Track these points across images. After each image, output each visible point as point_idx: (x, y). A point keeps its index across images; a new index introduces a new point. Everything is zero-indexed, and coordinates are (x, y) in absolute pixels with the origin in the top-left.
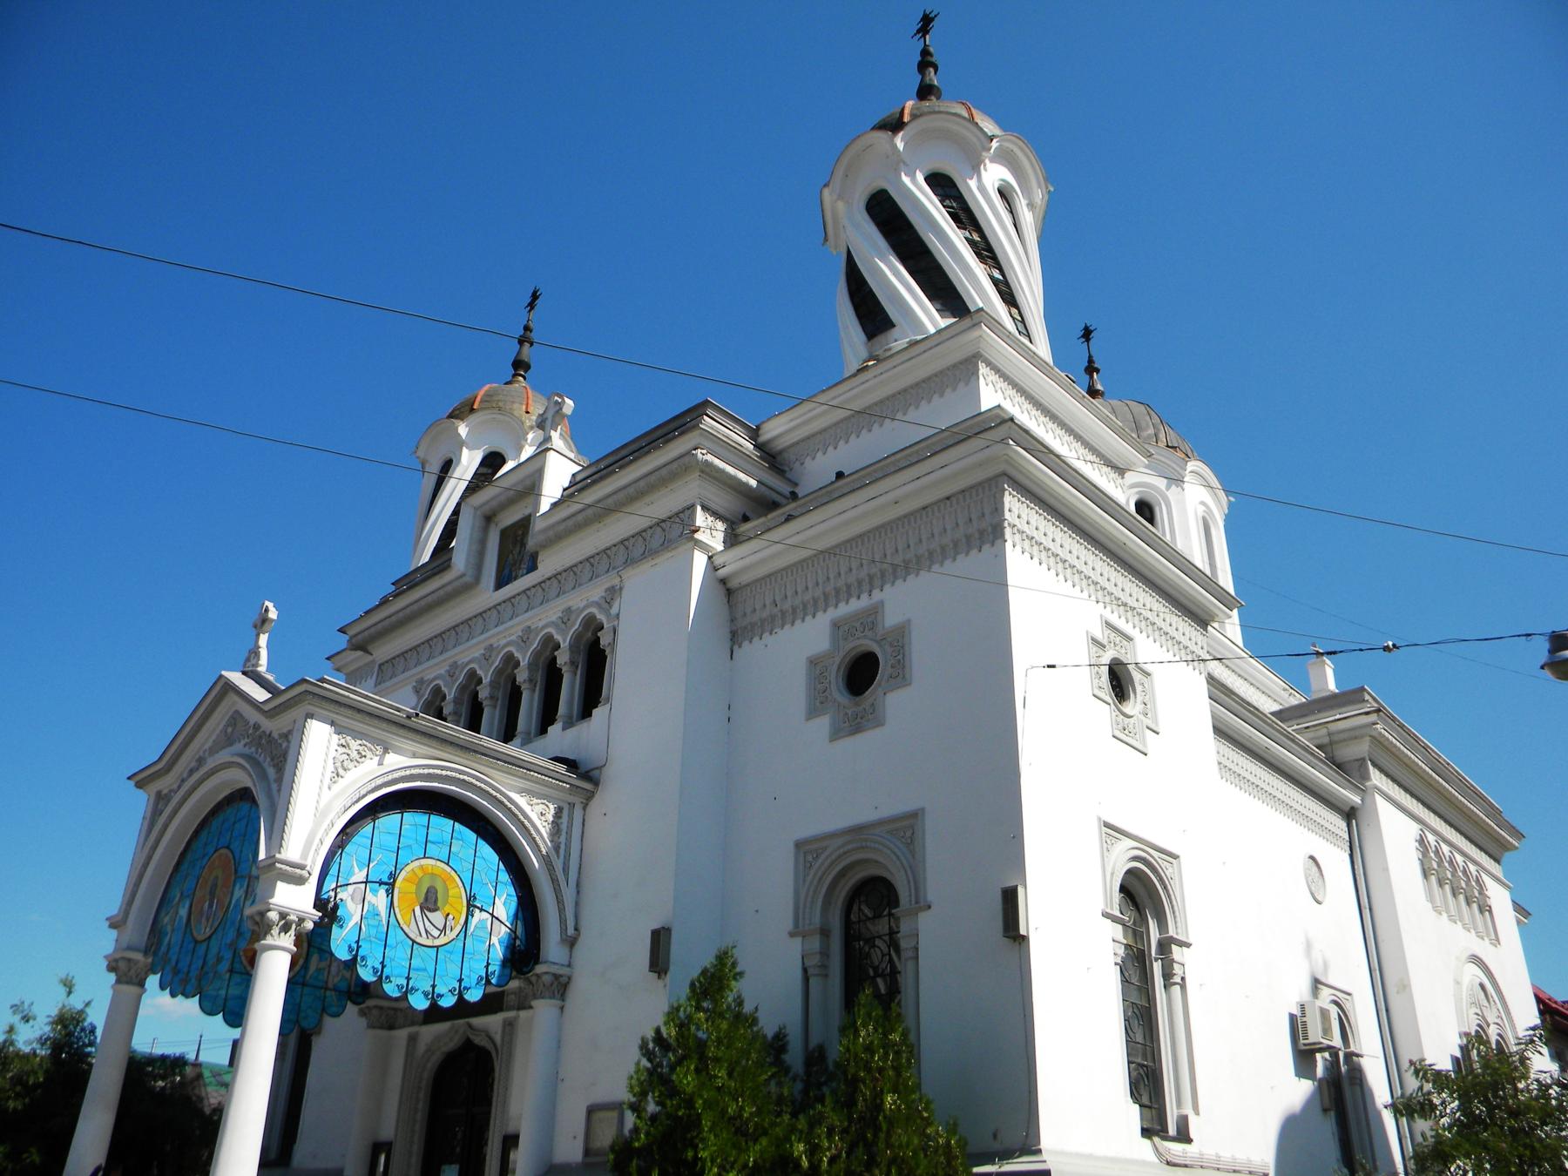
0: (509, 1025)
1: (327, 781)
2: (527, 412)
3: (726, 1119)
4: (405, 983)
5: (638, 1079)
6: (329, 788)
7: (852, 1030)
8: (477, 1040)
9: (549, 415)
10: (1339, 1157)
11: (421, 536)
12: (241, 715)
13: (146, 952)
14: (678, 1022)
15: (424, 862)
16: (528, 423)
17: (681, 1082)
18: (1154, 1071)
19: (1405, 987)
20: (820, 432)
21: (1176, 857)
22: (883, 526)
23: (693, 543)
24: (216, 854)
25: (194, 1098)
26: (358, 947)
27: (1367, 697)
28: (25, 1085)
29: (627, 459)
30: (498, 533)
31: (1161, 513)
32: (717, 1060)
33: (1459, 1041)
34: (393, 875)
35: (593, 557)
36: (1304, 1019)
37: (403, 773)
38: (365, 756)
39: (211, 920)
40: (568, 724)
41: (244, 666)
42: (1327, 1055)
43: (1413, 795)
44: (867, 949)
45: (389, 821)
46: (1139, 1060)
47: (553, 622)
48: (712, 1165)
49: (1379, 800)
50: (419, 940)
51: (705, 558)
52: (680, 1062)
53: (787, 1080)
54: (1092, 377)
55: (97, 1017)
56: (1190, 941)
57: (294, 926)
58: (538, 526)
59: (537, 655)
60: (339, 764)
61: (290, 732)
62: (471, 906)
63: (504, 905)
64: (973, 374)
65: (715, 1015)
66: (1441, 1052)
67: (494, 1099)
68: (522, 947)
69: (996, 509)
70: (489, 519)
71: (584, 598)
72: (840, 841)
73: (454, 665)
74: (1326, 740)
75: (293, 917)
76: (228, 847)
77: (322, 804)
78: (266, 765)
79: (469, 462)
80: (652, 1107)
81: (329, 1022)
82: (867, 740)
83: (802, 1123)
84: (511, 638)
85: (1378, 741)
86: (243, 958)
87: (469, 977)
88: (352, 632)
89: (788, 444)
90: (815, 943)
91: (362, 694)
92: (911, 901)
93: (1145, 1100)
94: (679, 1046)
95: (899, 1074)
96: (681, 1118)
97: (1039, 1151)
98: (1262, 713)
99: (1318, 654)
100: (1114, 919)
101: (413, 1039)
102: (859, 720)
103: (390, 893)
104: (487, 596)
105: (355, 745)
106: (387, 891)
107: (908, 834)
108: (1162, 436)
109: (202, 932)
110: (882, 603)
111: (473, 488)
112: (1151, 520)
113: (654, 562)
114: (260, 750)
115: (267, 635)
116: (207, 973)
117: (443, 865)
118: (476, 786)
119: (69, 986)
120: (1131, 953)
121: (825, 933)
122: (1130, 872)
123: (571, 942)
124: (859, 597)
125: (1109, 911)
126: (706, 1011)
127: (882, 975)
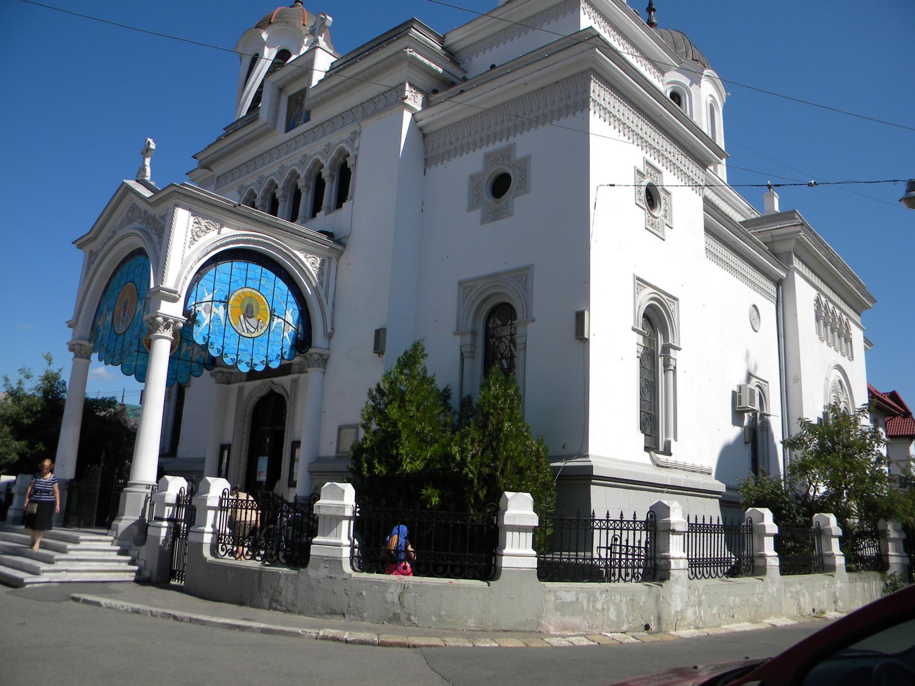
0: (295, 382)
1: (188, 244)
2: (304, 25)
3: (415, 433)
4: (235, 357)
5: (367, 411)
6: (190, 247)
7: (487, 387)
8: (277, 390)
9: (317, 27)
10: (751, 468)
11: (240, 100)
12: (137, 206)
13: (90, 341)
14: (389, 380)
15: (245, 290)
16: (304, 32)
17: (390, 413)
18: (654, 417)
19: (798, 380)
20: (482, 40)
21: (676, 299)
22: (518, 97)
23: (403, 106)
24: (126, 285)
25: (122, 421)
26: (209, 337)
27: (796, 216)
28: (31, 412)
29: (364, 54)
30: (287, 98)
31: (686, 100)
32: (410, 401)
33: (823, 410)
34: (228, 298)
35: (343, 113)
36: (740, 394)
37: (232, 239)
38: (210, 229)
39: (125, 323)
40: (329, 212)
41: (137, 177)
42: (751, 414)
43: (816, 274)
44: (497, 343)
45: (225, 267)
46: (646, 411)
47: (319, 152)
48: (407, 457)
49: (796, 275)
50: (243, 334)
51: (410, 115)
52: (390, 402)
53: (450, 414)
54: (650, 14)
55: (66, 377)
56: (680, 347)
57: (172, 326)
58: (310, 94)
59: (310, 171)
60: (194, 234)
61: (166, 215)
62: (272, 315)
63: (291, 315)
64: (576, 7)
65: (411, 377)
66: (813, 411)
67: (287, 421)
68: (302, 339)
69: (585, 90)
70: (281, 90)
71: (338, 138)
73: (262, 177)
74: (770, 240)
75: (171, 320)
76: (132, 282)
77: (186, 257)
78: (152, 234)
79: (269, 54)
80: (374, 426)
81: (194, 380)
82: (502, 224)
83: (457, 437)
84: (295, 161)
85: (800, 242)
86: (144, 345)
87: (272, 355)
88: (200, 158)
89: (461, 47)
90: (468, 339)
91: (209, 194)
92: (523, 317)
93: (648, 432)
94: (390, 393)
95: (512, 412)
96: (390, 432)
97: (588, 456)
98: (734, 222)
99: (769, 187)
100: (638, 332)
101: (241, 389)
102: (498, 212)
103: (226, 307)
104: (280, 136)
105: (203, 222)
106: (224, 306)
107: (524, 279)
108: (690, 53)
109: (120, 329)
110: (515, 144)
111: (270, 72)
112: (679, 104)
113: (378, 117)
114: (148, 226)
115: (150, 158)
116: (124, 352)
117: (255, 292)
118: (274, 246)
119: (50, 361)
120: (647, 352)
121: (474, 333)
122: (649, 306)
123: (330, 336)
124: (501, 141)
125: (636, 327)
126: (405, 375)
127: (506, 358)
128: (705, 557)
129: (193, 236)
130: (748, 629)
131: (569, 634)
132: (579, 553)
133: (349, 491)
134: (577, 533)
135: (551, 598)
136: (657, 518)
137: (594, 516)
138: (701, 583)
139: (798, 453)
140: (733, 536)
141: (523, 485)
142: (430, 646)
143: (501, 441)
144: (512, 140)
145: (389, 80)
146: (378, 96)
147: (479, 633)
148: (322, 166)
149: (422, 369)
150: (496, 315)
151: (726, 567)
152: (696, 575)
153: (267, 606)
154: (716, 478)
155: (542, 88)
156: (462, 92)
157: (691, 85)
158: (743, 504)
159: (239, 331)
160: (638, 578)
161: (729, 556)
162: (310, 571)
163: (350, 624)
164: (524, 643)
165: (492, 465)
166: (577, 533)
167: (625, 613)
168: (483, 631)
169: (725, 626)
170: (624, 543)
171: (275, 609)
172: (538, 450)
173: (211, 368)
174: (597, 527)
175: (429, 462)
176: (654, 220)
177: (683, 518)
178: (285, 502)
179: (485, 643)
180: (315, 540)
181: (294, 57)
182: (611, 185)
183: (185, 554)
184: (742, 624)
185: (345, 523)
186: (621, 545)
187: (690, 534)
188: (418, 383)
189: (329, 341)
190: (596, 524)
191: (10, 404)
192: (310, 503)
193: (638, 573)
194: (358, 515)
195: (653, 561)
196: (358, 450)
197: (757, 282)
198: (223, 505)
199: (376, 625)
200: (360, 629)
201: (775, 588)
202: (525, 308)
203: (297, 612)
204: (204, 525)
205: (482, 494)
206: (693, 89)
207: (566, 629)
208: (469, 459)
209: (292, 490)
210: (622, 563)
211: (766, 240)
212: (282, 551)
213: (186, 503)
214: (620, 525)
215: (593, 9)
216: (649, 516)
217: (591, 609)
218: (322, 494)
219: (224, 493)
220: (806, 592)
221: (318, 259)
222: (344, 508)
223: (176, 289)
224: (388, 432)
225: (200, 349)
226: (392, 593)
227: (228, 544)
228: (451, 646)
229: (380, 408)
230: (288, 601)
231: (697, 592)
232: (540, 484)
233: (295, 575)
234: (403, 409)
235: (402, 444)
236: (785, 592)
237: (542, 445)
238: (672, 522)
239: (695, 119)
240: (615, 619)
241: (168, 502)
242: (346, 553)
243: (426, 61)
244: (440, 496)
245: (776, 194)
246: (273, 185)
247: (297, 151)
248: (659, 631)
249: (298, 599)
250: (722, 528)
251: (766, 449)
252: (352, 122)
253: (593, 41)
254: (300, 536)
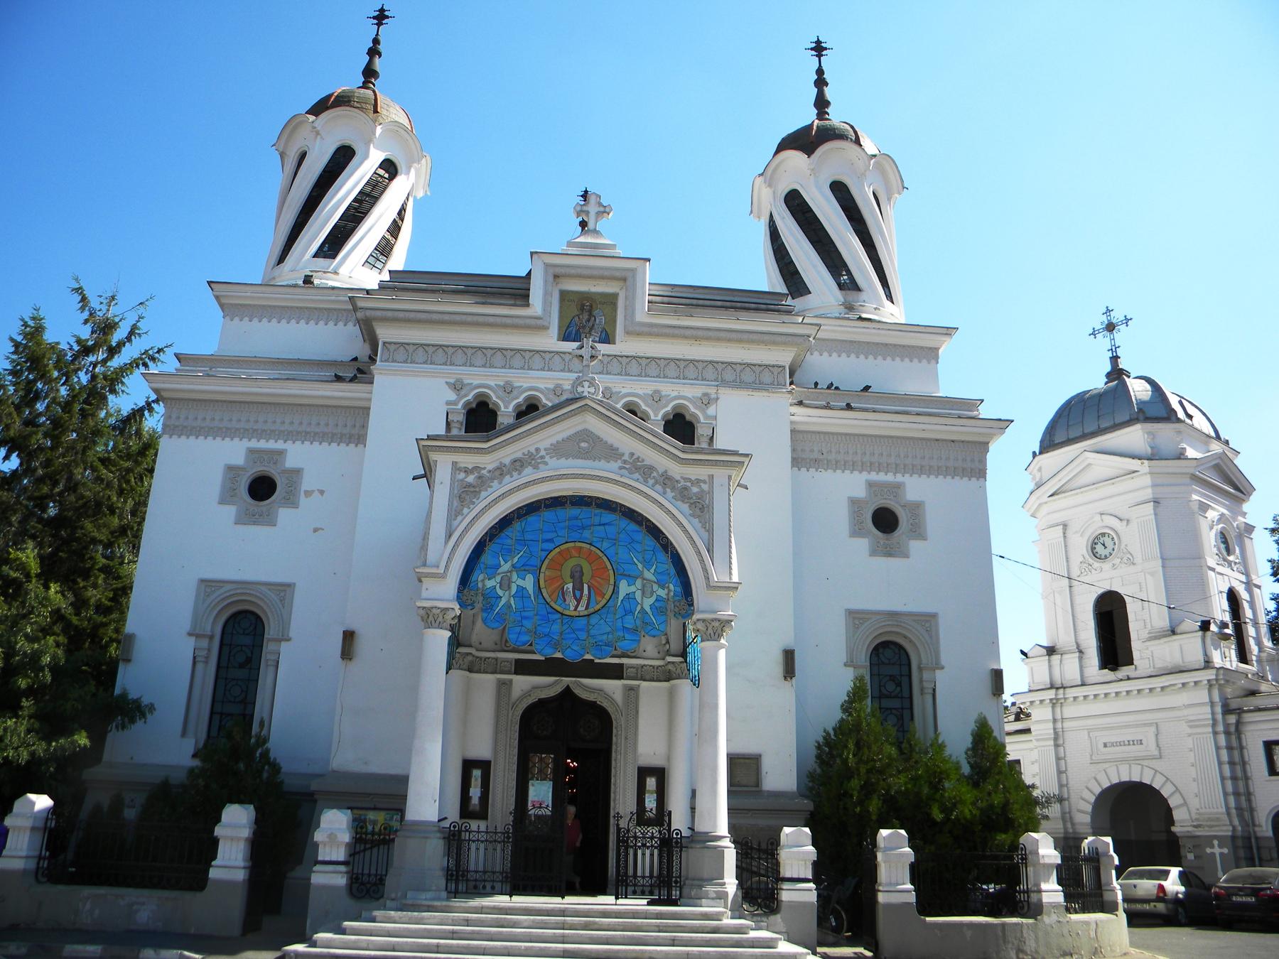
72: (234, 586)
191: (895, 756)
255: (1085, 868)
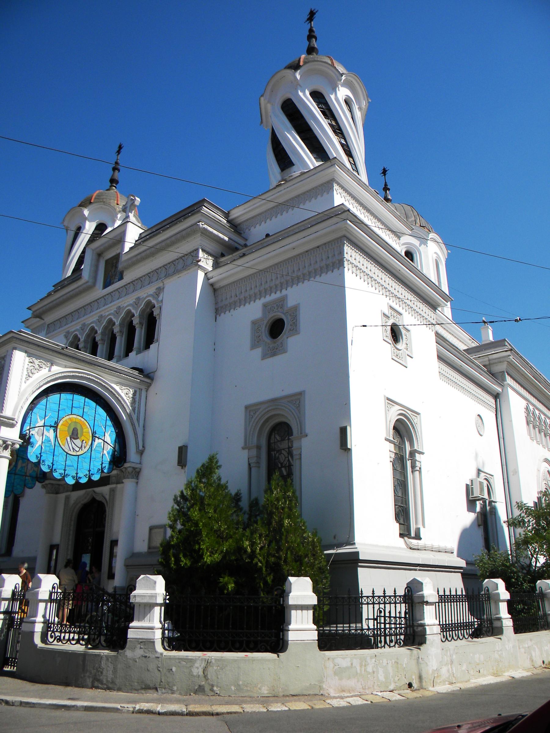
0: (113, 491)
1: (24, 379)
2: (118, 204)
4: (63, 472)
5: (173, 514)
6: (25, 382)
14: (191, 488)
18: (406, 509)
19: (516, 472)
20: (258, 215)
21: (418, 414)
26: (41, 456)
27: (506, 344)
31: (417, 257)
32: (209, 505)
33: (537, 495)
34: (57, 423)
35: (150, 273)
36: (472, 486)
37: (60, 375)
38: (42, 367)
40: (139, 352)
42: (481, 502)
45: (54, 398)
46: (399, 504)
47: (131, 304)
48: (207, 552)
49: (510, 391)
50: (69, 452)
51: (203, 274)
52: (192, 506)
53: (241, 513)
54: (386, 192)
57: (10, 447)
58: (123, 258)
59: (123, 319)
60: (29, 371)
61: (5, 356)
62: (94, 436)
63: (110, 436)
65: (208, 485)
67: (106, 524)
68: (118, 455)
69: (341, 253)
70: (100, 255)
74: (487, 363)
75: (9, 443)
79: (90, 227)
80: (179, 526)
83: (248, 533)
85: (510, 364)
90: (254, 452)
91: (40, 338)
93: (402, 522)
94: (192, 499)
96: (193, 531)
97: (354, 544)
98: (459, 350)
101: (67, 498)
102: (275, 350)
103: (55, 431)
104: (99, 292)
106: (54, 430)
107: (298, 403)
108: (418, 221)
110: (286, 296)
111: (90, 241)
117: (80, 418)
118: (95, 381)
121: (259, 447)
122: (397, 420)
123: (141, 453)
124: (276, 293)
125: (388, 438)
126: (204, 483)
127: (285, 467)
128: (453, 622)
129: (28, 373)
130: (492, 682)
131: (346, 695)
132: (351, 625)
133: (160, 581)
134: (349, 609)
135: (330, 664)
136: (413, 593)
137: (362, 594)
138: (452, 645)
139: (520, 530)
140: (475, 603)
141: (303, 570)
142: (231, 713)
143: (283, 534)
144: (284, 292)
145: (185, 248)
146: (177, 259)
147: (271, 699)
148: (133, 316)
149: (217, 478)
150: (276, 432)
151: (470, 630)
152: (447, 638)
153: (90, 684)
154: (458, 556)
155: (307, 252)
156: (244, 255)
157: (420, 245)
158: (480, 576)
159: (66, 451)
160: (400, 643)
161: (473, 621)
162: (128, 653)
163: (162, 697)
164: (309, 706)
165: (277, 555)
166: (349, 609)
167: (391, 674)
168: (275, 697)
169: (473, 681)
170: (387, 615)
171: (97, 688)
172: (313, 540)
173: (42, 481)
174: (365, 602)
175: (225, 555)
176: (398, 352)
177: (434, 591)
178: (105, 592)
179: (277, 707)
180: (131, 625)
181: (109, 229)
182: (364, 326)
183: (18, 642)
184: (486, 678)
185: (157, 609)
186: (385, 617)
187: (440, 604)
188: (215, 490)
189: (141, 457)
190: (364, 601)
192: (127, 592)
193: (400, 639)
194: (168, 601)
195: (411, 629)
196: (167, 546)
197: (480, 397)
198: (53, 598)
199: (185, 696)
200: (171, 702)
201: (511, 645)
202: (299, 426)
203: (116, 689)
204: (36, 616)
205: (269, 579)
206: (422, 248)
207: (343, 691)
208: (258, 551)
209: (111, 581)
210: (387, 632)
211: (484, 363)
212: (103, 635)
213: (20, 597)
214: (383, 600)
215: (343, 190)
216: (406, 591)
217: (363, 672)
218: (137, 585)
219: (53, 588)
220: (536, 647)
221: (131, 390)
222: (156, 596)
223: (13, 417)
224: (191, 530)
225: (33, 466)
226: (198, 668)
227: (57, 631)
228: (248, 712)
229: (184, 511)
230: (109, 679)
231: (449, 652)
232: (317, 568)
233: (114, 656)
234: (203, 511)
235: (203, 541)
236: (519, 648)
237: (316, 536)
238: (425, 595)
239: (424, 272)
240: (384, 680)
241: (4, 597)
242: (158, 635)
243: (215, 232)
244: (235, 583)
245: (490, 327)
246: (93, 331)
247: (112, 304)
248: (421, 688)
249: (117, 677)
250: (465, 597)
251: (496, 538)
252: (157, 280)
253: (344, 216)
254: (118, 621)
255: (486, 604)
